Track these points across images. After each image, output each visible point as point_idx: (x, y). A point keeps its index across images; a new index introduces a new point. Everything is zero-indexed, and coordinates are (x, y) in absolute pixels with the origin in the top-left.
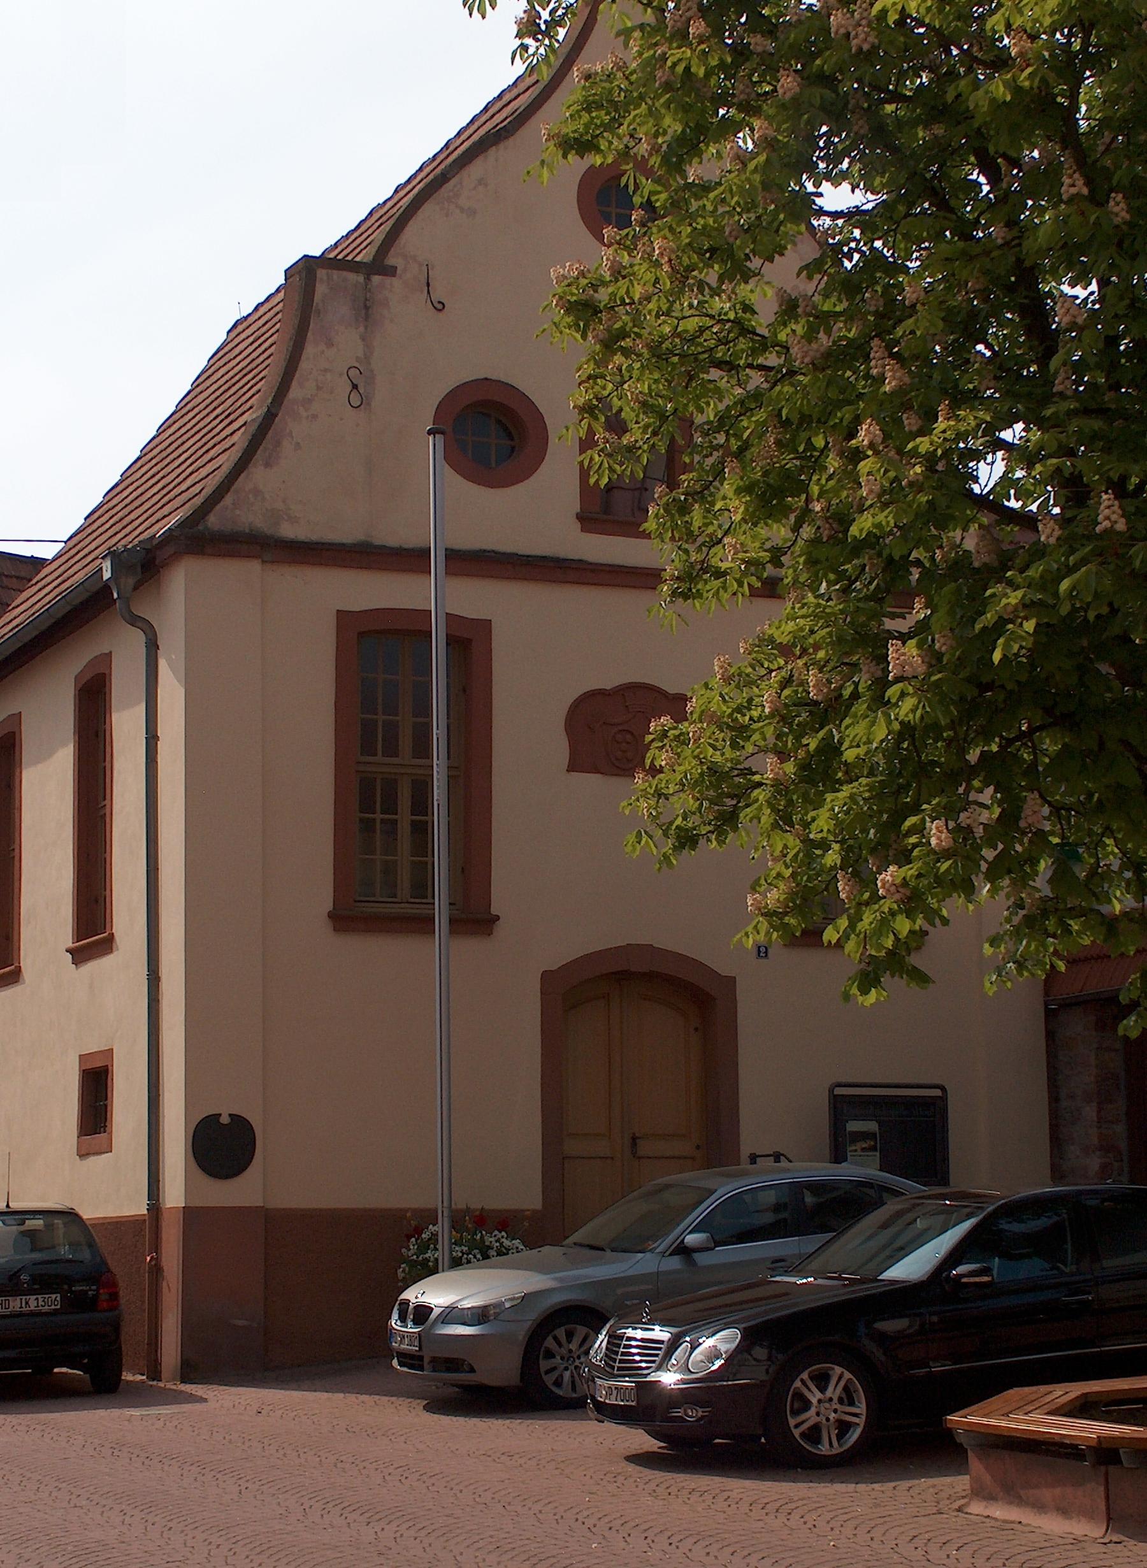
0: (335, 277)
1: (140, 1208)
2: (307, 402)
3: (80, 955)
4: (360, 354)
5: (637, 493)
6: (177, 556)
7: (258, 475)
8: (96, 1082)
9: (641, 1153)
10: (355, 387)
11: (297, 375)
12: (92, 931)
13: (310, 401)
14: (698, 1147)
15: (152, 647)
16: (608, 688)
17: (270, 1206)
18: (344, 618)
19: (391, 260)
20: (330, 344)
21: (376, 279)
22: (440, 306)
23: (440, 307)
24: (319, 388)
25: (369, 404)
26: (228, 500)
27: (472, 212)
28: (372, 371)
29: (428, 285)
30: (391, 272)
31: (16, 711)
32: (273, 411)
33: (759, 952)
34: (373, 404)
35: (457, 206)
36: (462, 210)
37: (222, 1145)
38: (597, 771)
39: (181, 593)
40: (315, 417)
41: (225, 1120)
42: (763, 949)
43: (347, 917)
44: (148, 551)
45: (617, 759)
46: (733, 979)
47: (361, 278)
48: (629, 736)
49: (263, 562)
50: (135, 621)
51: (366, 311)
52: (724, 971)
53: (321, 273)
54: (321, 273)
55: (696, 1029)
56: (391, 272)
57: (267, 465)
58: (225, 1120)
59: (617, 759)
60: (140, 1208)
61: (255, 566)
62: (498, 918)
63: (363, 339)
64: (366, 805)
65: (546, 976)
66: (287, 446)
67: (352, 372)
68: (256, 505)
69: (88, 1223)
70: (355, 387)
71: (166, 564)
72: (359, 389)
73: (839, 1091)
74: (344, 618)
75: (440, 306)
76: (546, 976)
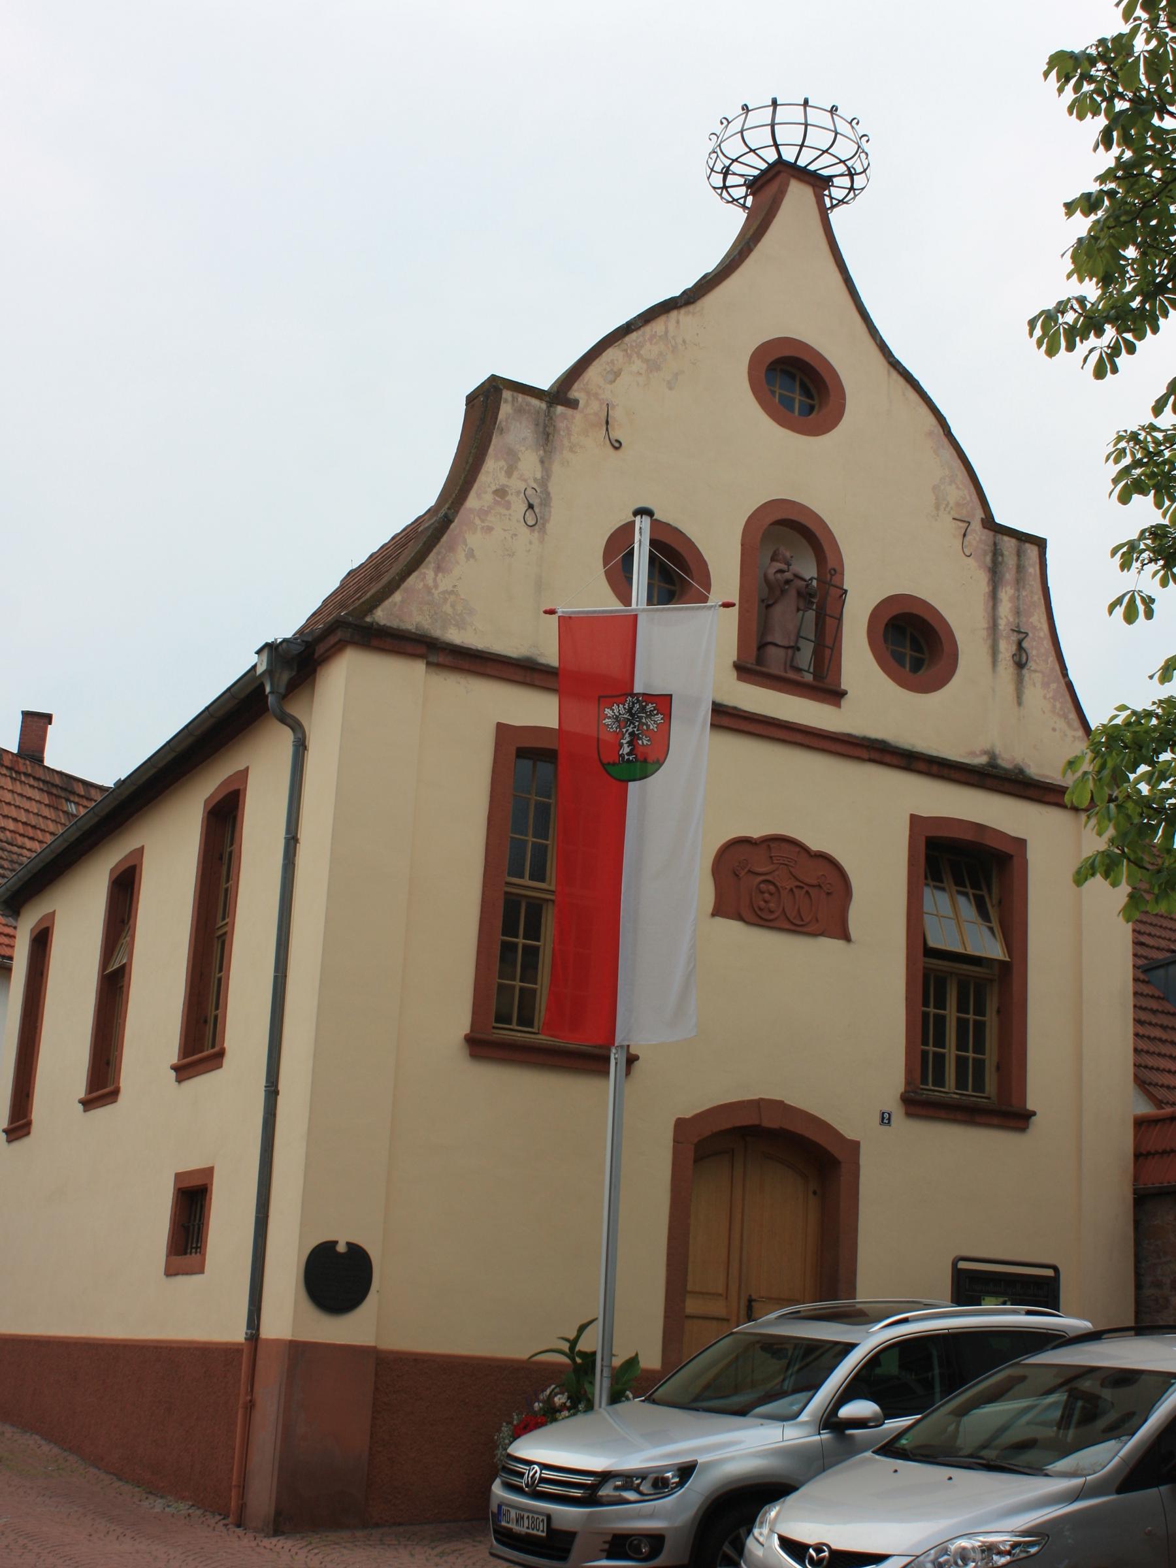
0: (520, 399)
1: (237, 1334)
3: (183, 1071)
4: (539, 476)
5: (790, 652)
6: (338, 649)
8: (192, 1200)
10: (531, 506)
11: (476, 486)
12: (201, 1047)
13: (487, 513)
15: (301, 746)
18: (503, 730)
21: (560, 409)
22: (617, 445)
23: (617, 445)
25: (544, 525)
26: (397, 597)
28: (548, 494)
29: (607, 423)
30: (573, 404)
33: (883, 1118)
34: (548, 526)
37: (337, 1276)
38: (740, 918)
39: (347, 677)
41: (341, 1248)
42: (886, 1116)
43: (481, 1045)
45: (761, 909)
47: (544, 406)
48: (771, 888)
49: (428, 664)
50: (287, 720)
51: (547, 436)
52: (850, 1134)
53: (507, 394)
54: (507, 394)
55: (815, 1193)
56: (573, 404)
58: (341, 1248)
60: (237, 1334)
61: (419, 667)
62: (1034, 1114)
63: (542, 462)
64: (509, 927)
65: (680, 1124)
67: (530, 492)
70: (531, 506)
71: (326, 659)
72: (536, 511)
73: (962, 1265)
74: (503, 730)
75: (617, 445)
76: (680, 1124)
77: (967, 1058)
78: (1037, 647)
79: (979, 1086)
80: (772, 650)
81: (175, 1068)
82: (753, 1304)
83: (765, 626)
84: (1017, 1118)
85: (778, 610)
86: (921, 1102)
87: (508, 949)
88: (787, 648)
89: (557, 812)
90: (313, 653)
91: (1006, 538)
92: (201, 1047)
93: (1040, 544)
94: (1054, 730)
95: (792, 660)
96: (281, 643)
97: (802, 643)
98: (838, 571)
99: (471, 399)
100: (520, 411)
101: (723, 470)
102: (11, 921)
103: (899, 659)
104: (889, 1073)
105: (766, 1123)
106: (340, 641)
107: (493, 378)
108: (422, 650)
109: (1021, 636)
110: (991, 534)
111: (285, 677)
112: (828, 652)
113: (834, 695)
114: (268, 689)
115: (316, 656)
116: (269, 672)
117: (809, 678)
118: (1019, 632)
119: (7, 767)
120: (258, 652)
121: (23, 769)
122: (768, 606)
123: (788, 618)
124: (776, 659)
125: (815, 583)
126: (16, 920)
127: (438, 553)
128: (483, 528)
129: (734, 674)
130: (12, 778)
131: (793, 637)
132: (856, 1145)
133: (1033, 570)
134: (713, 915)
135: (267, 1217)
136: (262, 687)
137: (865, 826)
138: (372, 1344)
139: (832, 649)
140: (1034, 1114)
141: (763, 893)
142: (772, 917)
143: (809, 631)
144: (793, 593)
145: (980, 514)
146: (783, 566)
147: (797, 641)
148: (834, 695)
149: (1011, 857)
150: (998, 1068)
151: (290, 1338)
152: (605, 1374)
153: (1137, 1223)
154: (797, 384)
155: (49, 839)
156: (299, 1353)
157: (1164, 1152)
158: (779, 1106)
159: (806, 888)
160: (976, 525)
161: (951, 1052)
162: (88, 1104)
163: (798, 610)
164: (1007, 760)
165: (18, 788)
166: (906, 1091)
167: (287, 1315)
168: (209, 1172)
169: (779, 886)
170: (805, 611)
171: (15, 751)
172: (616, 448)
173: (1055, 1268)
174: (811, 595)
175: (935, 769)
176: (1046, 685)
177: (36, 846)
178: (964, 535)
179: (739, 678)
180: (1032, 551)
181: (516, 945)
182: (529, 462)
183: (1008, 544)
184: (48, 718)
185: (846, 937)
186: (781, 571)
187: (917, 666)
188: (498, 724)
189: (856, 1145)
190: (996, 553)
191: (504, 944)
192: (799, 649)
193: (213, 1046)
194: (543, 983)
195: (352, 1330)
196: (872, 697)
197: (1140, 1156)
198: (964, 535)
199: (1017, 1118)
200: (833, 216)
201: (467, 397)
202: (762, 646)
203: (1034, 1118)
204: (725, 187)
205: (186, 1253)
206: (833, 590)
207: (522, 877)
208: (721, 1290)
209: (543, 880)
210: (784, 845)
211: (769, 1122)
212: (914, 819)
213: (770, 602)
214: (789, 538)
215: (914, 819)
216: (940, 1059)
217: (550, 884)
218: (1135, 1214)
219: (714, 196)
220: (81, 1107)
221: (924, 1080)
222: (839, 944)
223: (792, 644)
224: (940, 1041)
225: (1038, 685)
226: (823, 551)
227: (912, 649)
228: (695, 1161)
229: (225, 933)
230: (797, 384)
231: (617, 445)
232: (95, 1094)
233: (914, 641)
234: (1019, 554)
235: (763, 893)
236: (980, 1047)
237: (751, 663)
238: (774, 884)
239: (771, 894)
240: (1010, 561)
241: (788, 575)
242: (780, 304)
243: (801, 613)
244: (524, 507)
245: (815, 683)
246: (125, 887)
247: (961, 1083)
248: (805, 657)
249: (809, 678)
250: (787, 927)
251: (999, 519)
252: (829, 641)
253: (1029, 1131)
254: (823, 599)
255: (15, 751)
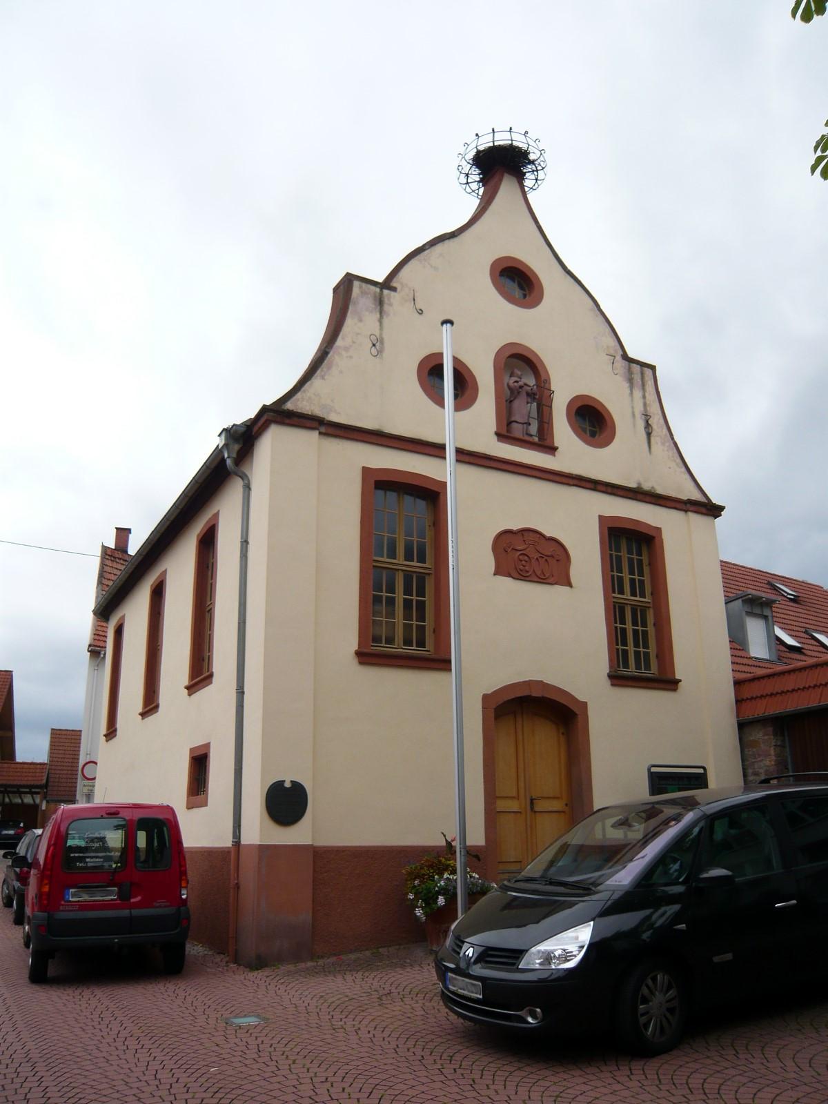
2: (347, 349)
3: (192, 689)
6: (265, 427)
7: (316, 383)
8: (200, 763)
9: (537, 809)
12: (200, 674)
14: (566, 805)
15: (248, 487)
16: (515, 529)
17: (317, 844)
18: (366, 471)
19: (394, 284)
20: (361, 320)
21: (386, 292)
22: (421, 312)
23: (421, 312)
24: (354, 342)
27: (436, 269)
30: (394, 289)
31: (164, 570)
32: (327, 350)
35: (429, 264)
36: (431, 266)
37: (286, 803)
38: (510, 576)
40: (351, 357)
41: (288, 785)
43: (365, 657)
44: (248, 426)
45: (521, 570)
46: (586, 703)
47: (378, 290)
48: (526, 558)
52: (581, 698)
53: (356, 283)
55: (563, 734)
56: (394, 289)
57: (323, 378)
58: (288, 785)
59: (521, 570)
60: (227, 842)
61: (315, 434)
62: (680, 681)
66: (334, 371)
68: (321, 399)
69: (185, 850)
72: (377, 344)
73: (653, 770)
74: (366, 471)
77: (640, 652)
78: (656, 421)
79: (648, 667)
80: (515, 425)
81: (188, 688)
82: (534, 801)
83: (510, 412)
84: (668, 682)
85: (516, 404)
86: (618, 679)
87: (377, 600)
88: (523, 424)
89: (402, 515)
90: (252, 432)
91: (635, 365)
92: (200, 674)
93: (653, 368)
94: (670, 468)
95: (527, 430)
96: (232, 427)
97: (531, 421)
98: (547, 381)
99: (336, 290)
100: (363, 293)
101: (480, 329)
102: (104, 624)
103: (584, 430)
104: (602, 664)
105: (534, 694)
106: (266, 421)
107: (348, 274)
108: (315, 424)
109: (647, 418)
110: (627, 362)
111: (236, 447)
112: (546, 425)
113: (552, 450)
114: (226, 456)
115: (253, 434)
116: (226, 445)
117: (536, 439)
118: (646, 415)
119: (109, 555)
120: (219, 435)
121: (117, 556)
122: (511, 401)
123: (524, 409)
124: (517, 430)
125: (535, 387)
126: (107, 623)
127: (322, 371)
128: (347, 357)
129: (495, 438)
130: (111, 560)
131: (527, 417)
132: (585, 705)
133: (650, 383)
134: (495, 574)
135: (241, 768)
136: (223, 461)
137: (575, 522)
138: (310, 843)
139: (548, 423)
140: (680, 681)
141: (521, 561)
142: (528, 575)
143: (534, 414)
144: (524, 394)
145: (621, 352)
146: (516, 379)
147: (528, 420)
148: (552, 450)
149: (654, 538)
150: (657, 656)
151: (259, 843)
152: (462, 854)
153: (741, 739)
154: (517, 280)
155: (118, 573)
156: (265, 851)
157: (772, 694)
158: (541, 683)
159: (546, 558)
160: (619, 358)
161: (631, 648)
162: (144, 715)
163: (528, 403)
164: (646, 486)
165: (115, 565)
166: (610, 672)
167: (257, 828)
168: (207, 746)
169: (529, 557)
170: (531, 403)
171: (114, 547)
172: (420, 314)
173: (704, 768)
174: (535, 394)
175: (609, 490)
176: (663, 444)
177: (114, 578)
178: (613, 363)
179: (498, 440)
180: (648, 372)
181: (382, 596)
182: (371, 320)
183: (636, 368)
184: (129, 531)
185: (570, 584)
186: (516, 382)
187: (593, 434)
188: (363, 467)
189: (585, 705)
190: (630, 371)
191: (374, 596)
192: (530, 424)
193: (208, 671)
194: (403, 616)
195: (299, 835)
196: (571, 451)
197: (739, 701)
198: (613, 363)
199: (668, 682)
200: (529, 196)
201: (334, 289)
202: (509, 423)
203: (680, 683)
204: (467, 183)
205: (198, 795)
206: (546, 391)
207: (383, 557)
208: (514, 794)
209: (395, 559)
210: (531, 533)
211: (536, 693)
212: (601, 517)
213: (512, 399)
214: (519, 363)
215: (601, 517)
216: (625, 653)
217: (399, 560)
218: (739, 733)
219: (460, 189)
220: (140, 717)
221: (619, 667)
222: (568, 588)
223: (526, 421)
224: (625, 643)
225: (659, 444)
226: (537, 370)
227: (590, 426)
228: (496, 718)
229: (211, 609)
230: (517, 280)
231: (421, 312)
232: (147, 709)
233: (592, 420)
234: (642, 374)
235: (521, 561)
236: (646, 646)
237: (504, 432)
238: (528, 556)
239: (526, 562)
240: (637, 377)
241: (521, 383)
242: (503, 238)
243: (529, 405)
244: (371, 345)
245: (540, 443)
246: (158, 593)
247: (638, 666)
248: (534, 429)
249: (536, 439)
250: (536, 580)
251: (631, 354)
252: (546, 420)
253: (678, 690)
254: (541, 396)
255: (114, 547)
